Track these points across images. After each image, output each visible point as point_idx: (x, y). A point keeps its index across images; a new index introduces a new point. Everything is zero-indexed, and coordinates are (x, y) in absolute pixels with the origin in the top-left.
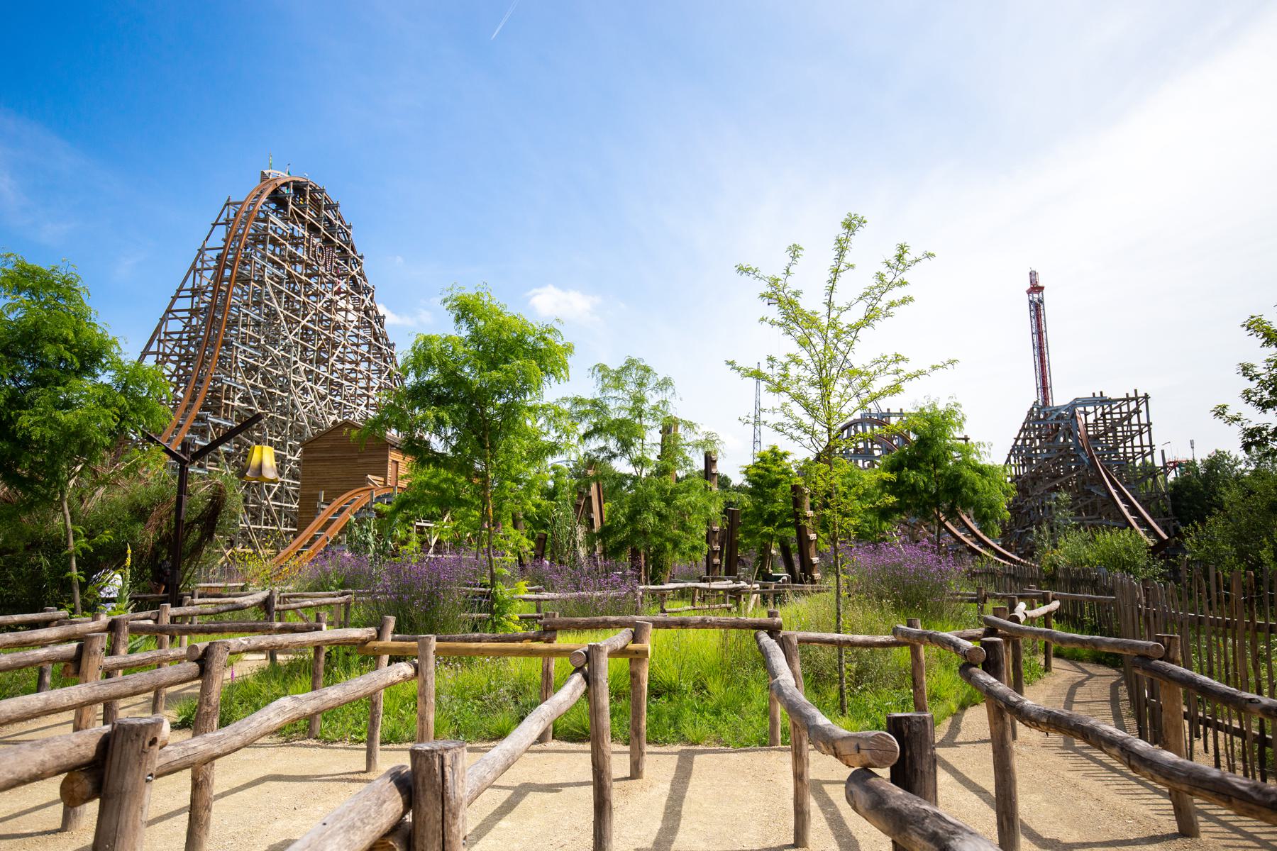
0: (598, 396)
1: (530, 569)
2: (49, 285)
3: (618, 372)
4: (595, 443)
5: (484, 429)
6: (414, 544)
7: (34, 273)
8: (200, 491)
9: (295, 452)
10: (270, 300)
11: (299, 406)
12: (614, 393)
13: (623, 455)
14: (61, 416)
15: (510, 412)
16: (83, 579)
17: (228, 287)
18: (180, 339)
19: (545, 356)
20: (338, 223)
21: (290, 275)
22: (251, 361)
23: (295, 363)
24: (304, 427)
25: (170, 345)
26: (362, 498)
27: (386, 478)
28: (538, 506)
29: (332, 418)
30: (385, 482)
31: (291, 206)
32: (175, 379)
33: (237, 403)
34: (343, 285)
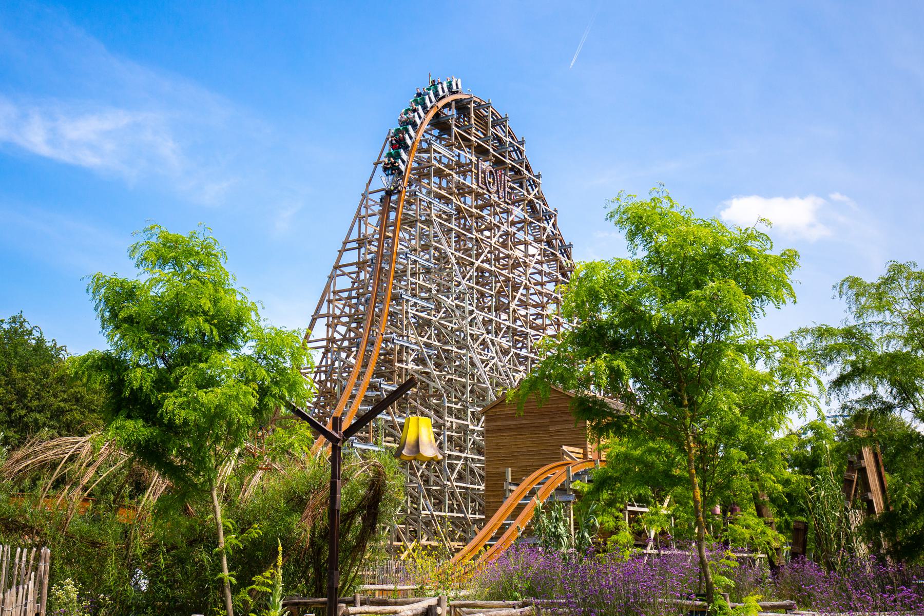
0: (852, 322)
1: (787, 572)
2: (189, 253)
3: (879, 286)
4: (857, 392)
5: (679, 380)
6: (625, 536)
7: (176, 242)
8: (357, 471)
9: (479, 420)
10: (439, 242)
11: (478, 363)
12: (877, 317)
13: (903, 406)
14: (202, 395)
15: (711, 354)
16: (234, 581)
17: (394, 232)
18: (350, 298)
19: (754, 274)
20: (509, 139)
21: (459, 210)
22: (423, 315)
23: (471, 312)
24: (485, 390)
25: (340, 305)
26: (558, 477)
27: (585, 449)
28: (786, 483)
29: (518, 376)
30: (585, 455)
31: (455, 129)
32: (346, 343)
33: (411, 366)
34: (518, 212)
